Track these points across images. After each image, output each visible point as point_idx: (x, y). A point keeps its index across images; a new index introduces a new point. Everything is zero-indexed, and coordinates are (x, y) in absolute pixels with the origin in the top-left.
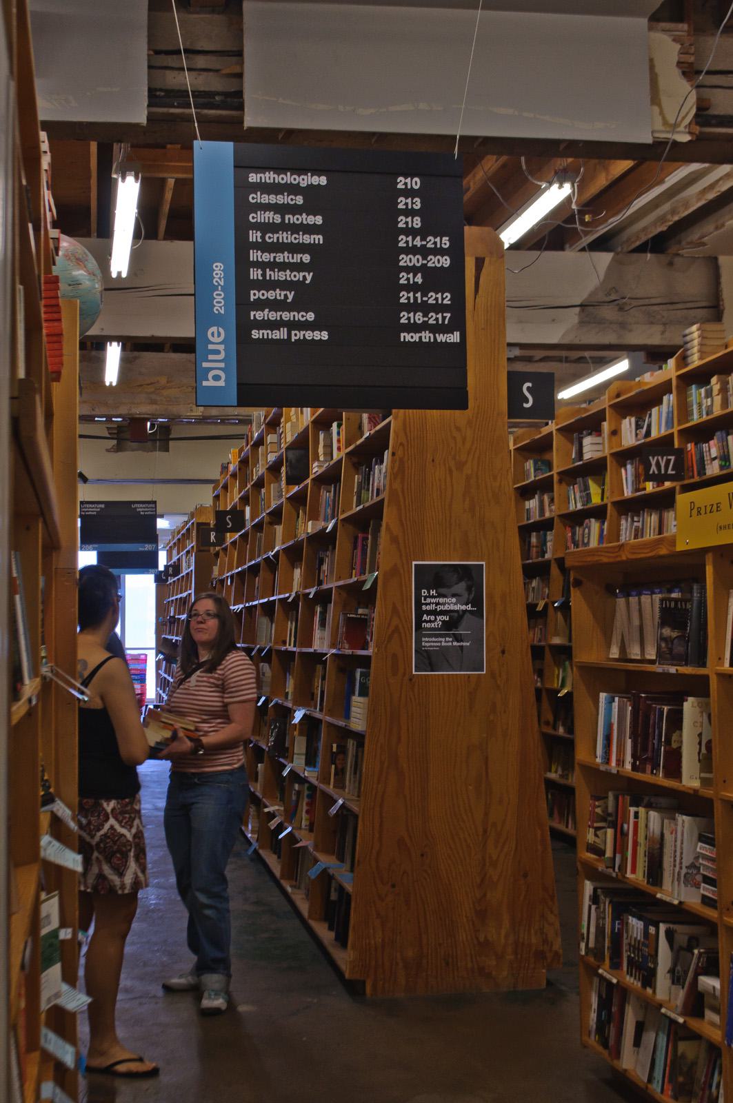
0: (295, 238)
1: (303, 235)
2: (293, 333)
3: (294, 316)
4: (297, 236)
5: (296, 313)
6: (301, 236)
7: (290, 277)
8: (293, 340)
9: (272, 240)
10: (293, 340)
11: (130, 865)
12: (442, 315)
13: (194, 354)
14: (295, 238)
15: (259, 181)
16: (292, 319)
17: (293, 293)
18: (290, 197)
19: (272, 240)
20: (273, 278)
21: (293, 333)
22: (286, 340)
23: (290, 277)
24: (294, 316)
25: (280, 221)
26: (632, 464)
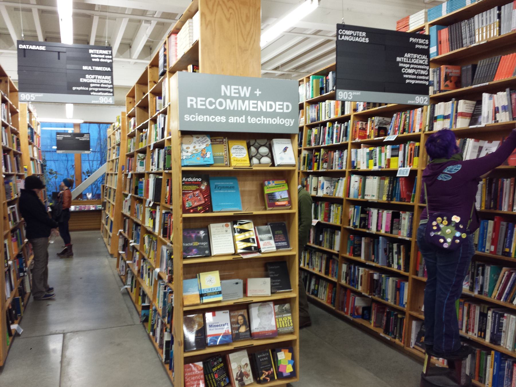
0: (193, 118)
1: (198, 115)
2: (244, 122)
3: (207, 118)
4: (194, 116)
5: (208, 117)
6: (197, 116)
7: (250, 121)
8: (244, 116)
9: (260, 122)
10: (244, 116)
11: (415, 126)
12: (93, 48)
13: (35, 3)
14: (193, 118)
15: (235, 121)
16: (205, 120)
17: (294, 120)
18: (281, 120)
19: (260, 122)
20: (265, 123)
21: (244, 122)
22: (197, 273)
23: (250, 121)
24: (207, 118)
25: (225, 120)
26: (339, 151)
